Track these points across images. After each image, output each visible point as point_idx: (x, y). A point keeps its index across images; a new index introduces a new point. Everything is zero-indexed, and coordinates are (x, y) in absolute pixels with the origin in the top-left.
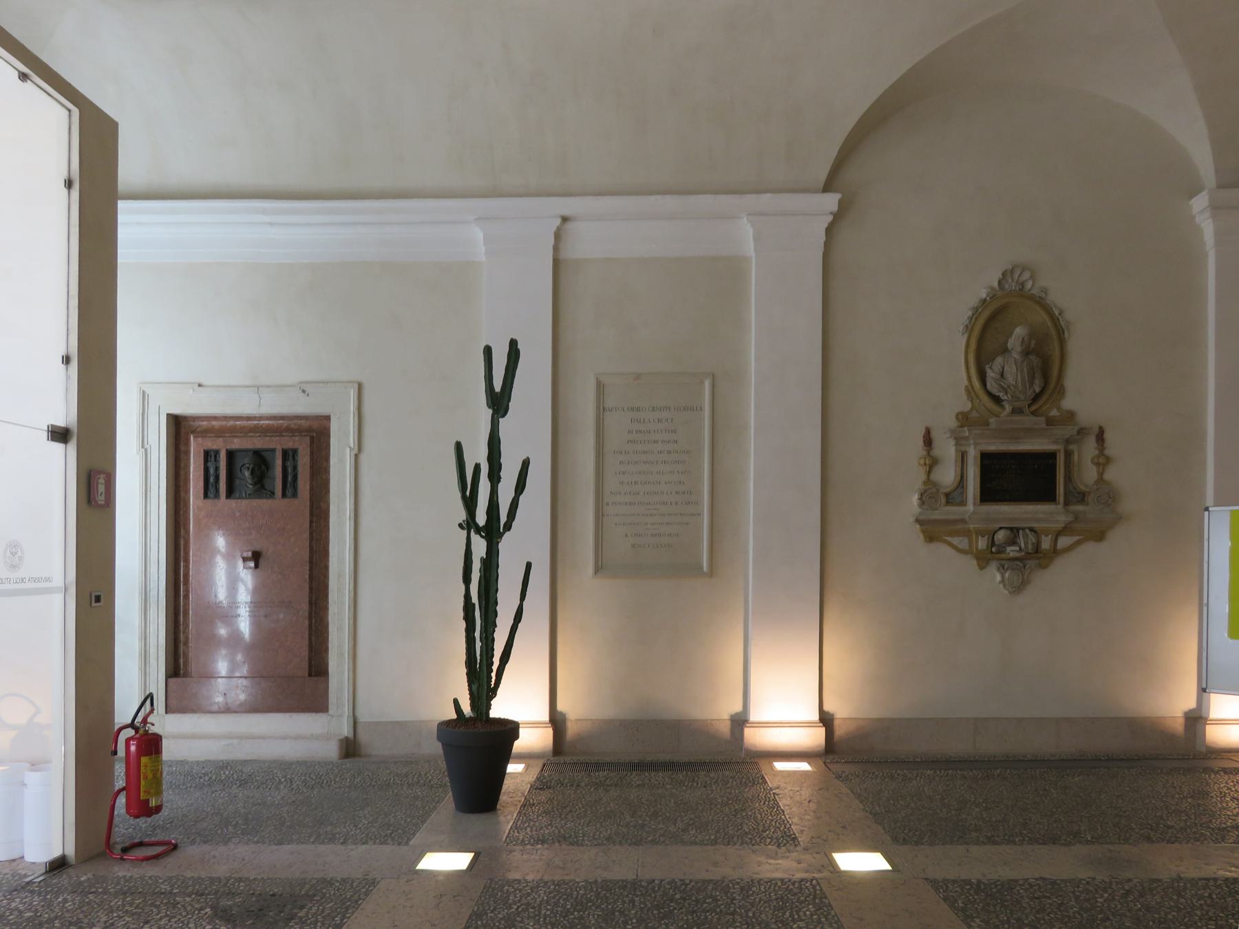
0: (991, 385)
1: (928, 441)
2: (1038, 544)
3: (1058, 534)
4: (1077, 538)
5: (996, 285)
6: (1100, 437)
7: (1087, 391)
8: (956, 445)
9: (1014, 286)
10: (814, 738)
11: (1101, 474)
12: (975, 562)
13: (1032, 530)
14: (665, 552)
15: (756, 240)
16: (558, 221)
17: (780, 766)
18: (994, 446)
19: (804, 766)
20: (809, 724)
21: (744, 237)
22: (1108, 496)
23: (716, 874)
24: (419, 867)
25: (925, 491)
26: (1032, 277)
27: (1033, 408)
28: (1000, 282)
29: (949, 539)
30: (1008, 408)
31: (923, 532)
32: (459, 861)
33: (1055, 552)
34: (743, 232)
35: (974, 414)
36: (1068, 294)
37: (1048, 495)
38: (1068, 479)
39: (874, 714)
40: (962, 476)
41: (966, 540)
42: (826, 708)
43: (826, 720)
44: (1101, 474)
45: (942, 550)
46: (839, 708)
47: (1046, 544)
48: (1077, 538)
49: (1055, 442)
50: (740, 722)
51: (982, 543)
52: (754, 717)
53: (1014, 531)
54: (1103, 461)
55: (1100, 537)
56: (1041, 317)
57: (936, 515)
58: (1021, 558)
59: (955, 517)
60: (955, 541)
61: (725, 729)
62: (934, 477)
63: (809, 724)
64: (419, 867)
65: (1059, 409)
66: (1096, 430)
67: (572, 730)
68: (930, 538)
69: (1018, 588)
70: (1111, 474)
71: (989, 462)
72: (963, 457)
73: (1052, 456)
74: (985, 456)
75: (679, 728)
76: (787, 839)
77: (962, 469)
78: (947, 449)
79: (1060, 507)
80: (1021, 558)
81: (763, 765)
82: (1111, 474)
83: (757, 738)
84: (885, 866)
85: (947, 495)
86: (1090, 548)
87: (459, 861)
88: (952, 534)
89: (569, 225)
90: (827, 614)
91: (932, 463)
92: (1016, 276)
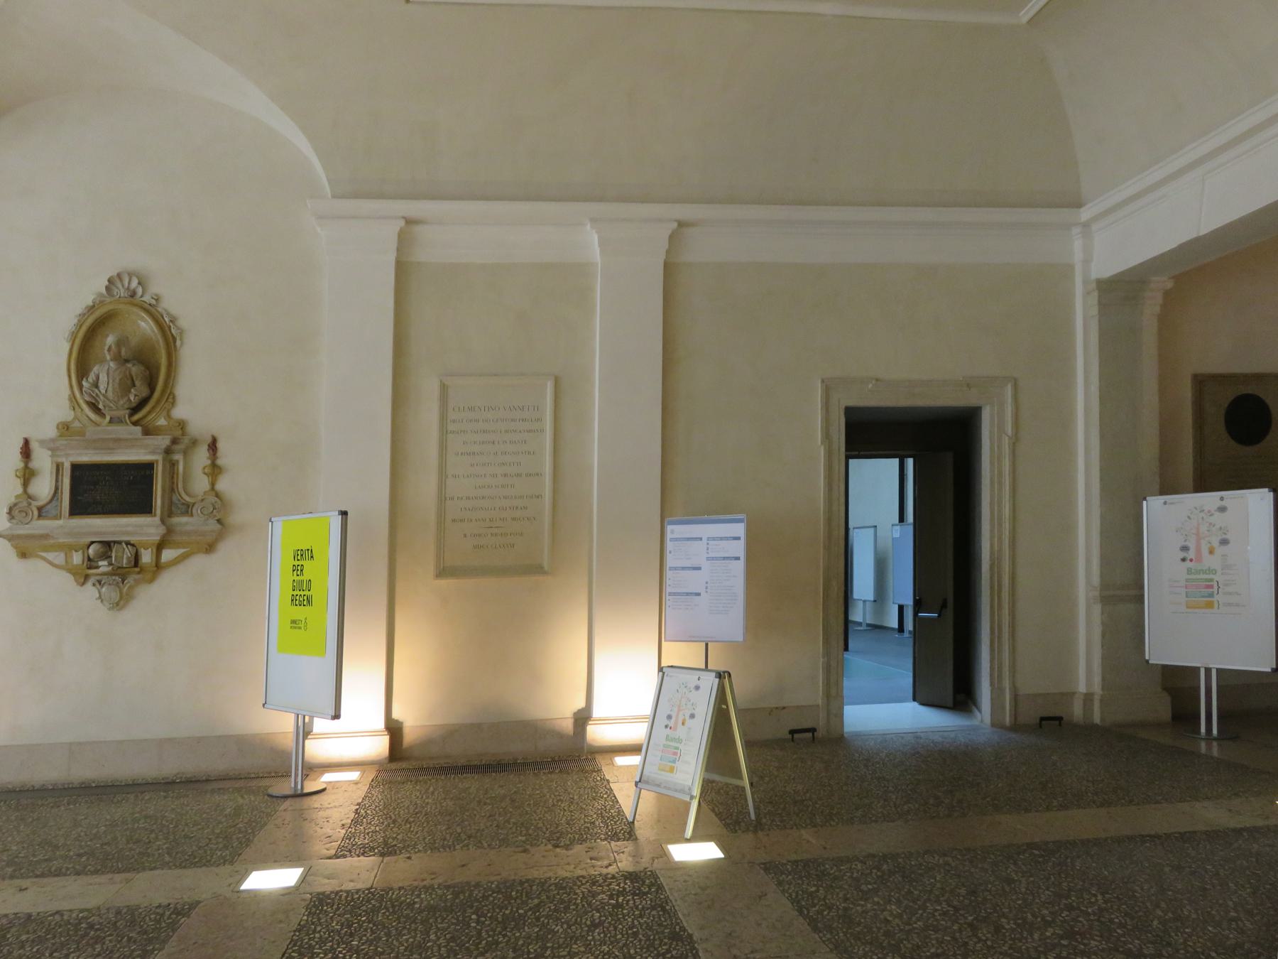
0: (144, 392)
1: (26, 452)
2: (137, 558)
3: (160, 547)
4: (181, 551)
5: (104, 291)
6: (213, 446)
7: (198, 398)
8: (52, 456)
9: (123, 293)
10: (378, 747)
11: (213, 485)
12: (72, 578)
13: (128, 543)
14: (492, 549)
15: (600, 245)
16: (675, 225)
17: (621, 761)
18: (86, 457)
19: (354, 775)
20: (373, 733)
21: (590, 243)
22: (219, 508)
23: (535, 874)
24: (243, 887)
25: (15, 505)
26: (139, 283)
27: (136, 417)
28: (107, 288)
29: (44, 554)
30: (108, 418)
31: (16, 547)
32: (709, 851)
33: (158, 566)
34: (587, 239)
35: (77, 424)
36: (177, 300)
37: (142, 506)
38: (171, 489)
39: (439, 721)
40: (57, 488)
41: (62, 555)
42: (397, 714)
43: (394, 730)
44: (213, 485)
45: (36, 566)
46: (411, 715)
47: (147, 557)
48: (181, 551)
49: (153, 453)
50: (583, 718)
51: (77, 558)
52: (597, 712)
53: (108, 545)
54: (215, 470)
55: (210, 548)
56: (146, 326)
57: (23, 530)
58: (120, 572)
59: (41, 532)
60: (50, 556)
61: (568, 726)
62: (32, 489)
63: (373, 733)
64: (243, 887)
65: (169, 416)
66: (209, 440)
67: (409, 736)
68: (23, 555)
69: (120, 604)
70: (223, 485)
71: (81, 474)
72: (59, 467)
73: (149, 466)
74: (76, 468)
75: (534, 729)
76: (628, 832)
77: (57, 481)
78: (43, 460)
79: (157, 520)
80: (120, 572)
81: (601, 761)
82: (223, 485)
83: (598, 734)
84: (718, 854)
85: (40, 509)
86: (199, 561)
87: (709, 851)
88: (47, 549)
89: (417, 229)
90: (595, 611)
91: (27, 475)
92: (126, 283)
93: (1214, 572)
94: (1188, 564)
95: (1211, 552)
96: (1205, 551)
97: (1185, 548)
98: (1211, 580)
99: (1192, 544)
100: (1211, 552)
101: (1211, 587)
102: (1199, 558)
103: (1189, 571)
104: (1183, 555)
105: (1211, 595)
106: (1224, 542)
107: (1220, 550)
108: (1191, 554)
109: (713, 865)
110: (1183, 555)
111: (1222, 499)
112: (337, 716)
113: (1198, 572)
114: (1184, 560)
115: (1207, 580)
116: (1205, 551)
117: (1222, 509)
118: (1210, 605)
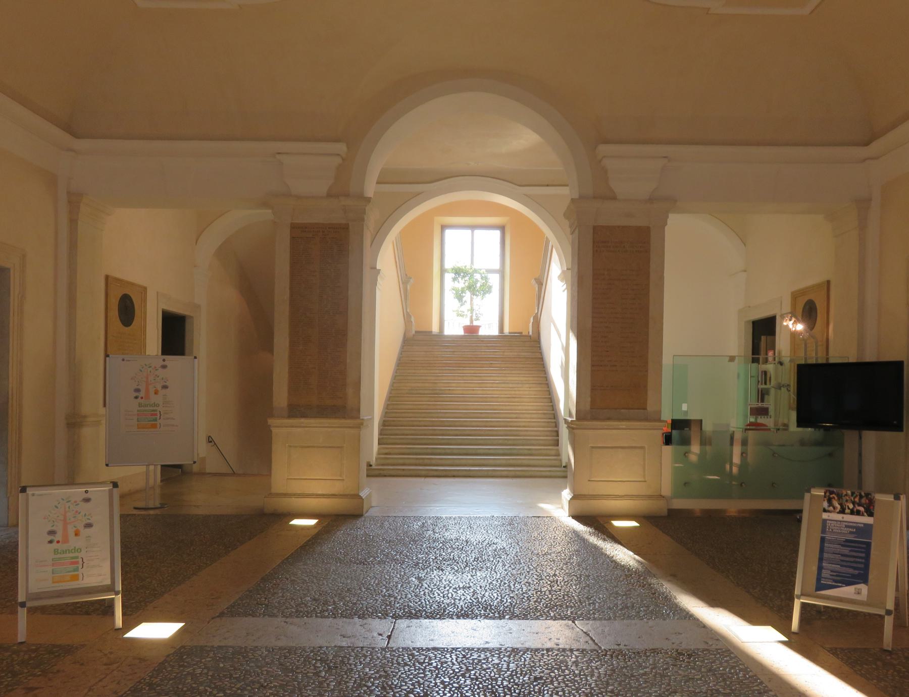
84: (637, 525)
93: (158, 405)
94: (139, 400)
95: (77, 534)
96: (71, 531)
97: (137, 390)
98: (77, 557)
99: (143, 388)
100: (156, 393)
101: (77, 563)
102: (66, 540)
103: (140, 405)
104: (50, 538)
105: (77, 570)
106: (165, 387)
107: (162, 392)
108: (142, 394)
109: (635, 527)
110: (50, 538)
111: (164, 360)
112: (368, 476)
113: (146, 406)
114: (136, 398)
115: (73, 558)
116: (71, 531)
117: (164, 367)
118: (154, 426)
